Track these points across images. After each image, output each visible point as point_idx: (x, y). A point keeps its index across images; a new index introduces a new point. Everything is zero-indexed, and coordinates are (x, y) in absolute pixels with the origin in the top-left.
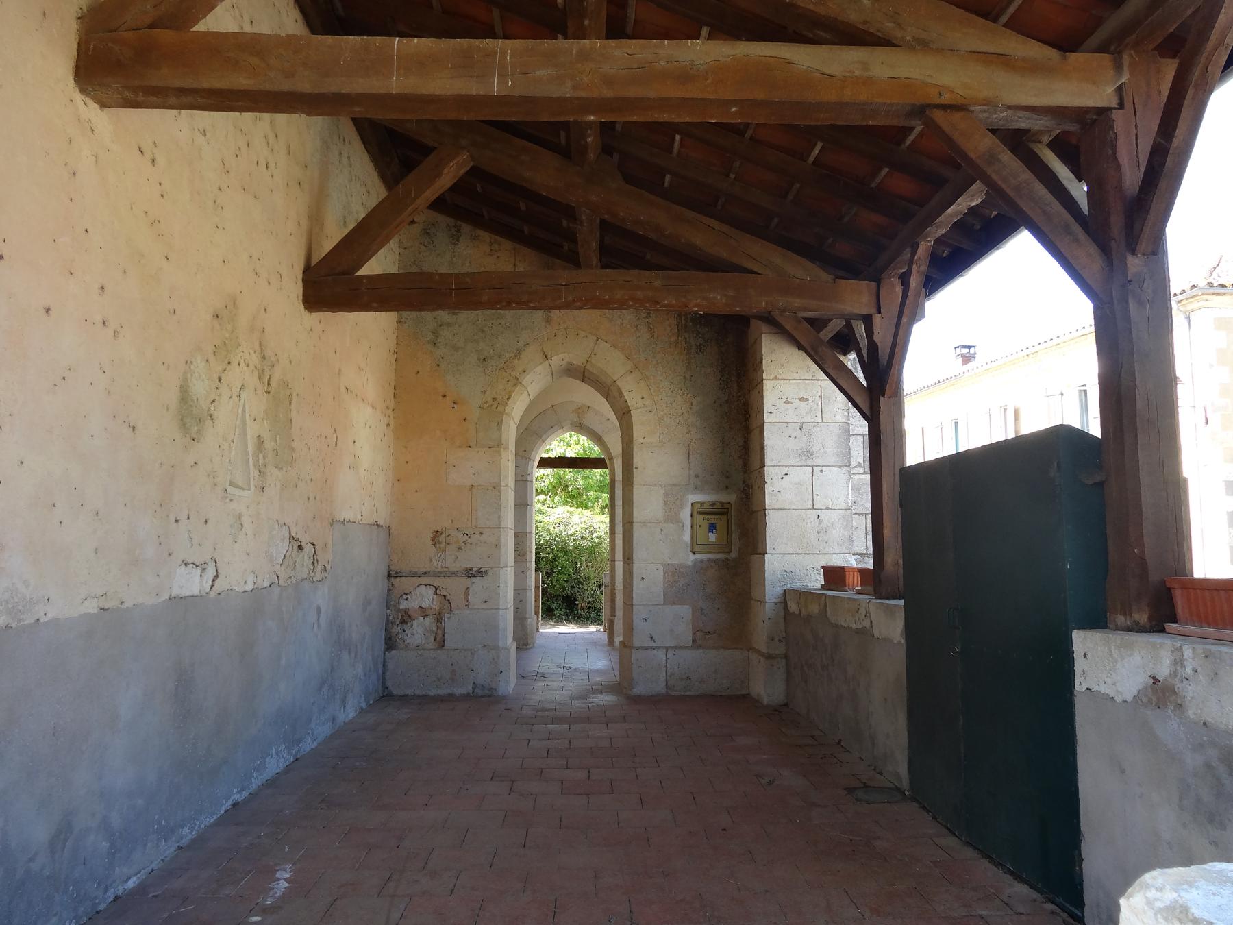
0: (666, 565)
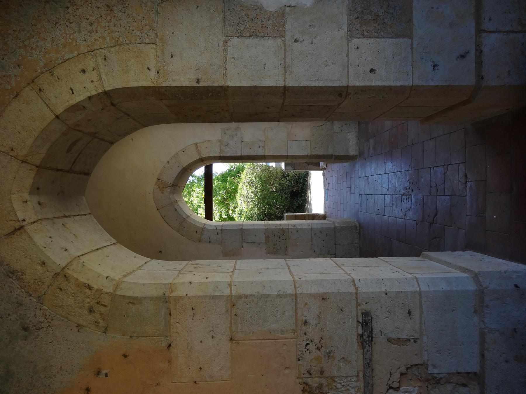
0: (351, 35)
